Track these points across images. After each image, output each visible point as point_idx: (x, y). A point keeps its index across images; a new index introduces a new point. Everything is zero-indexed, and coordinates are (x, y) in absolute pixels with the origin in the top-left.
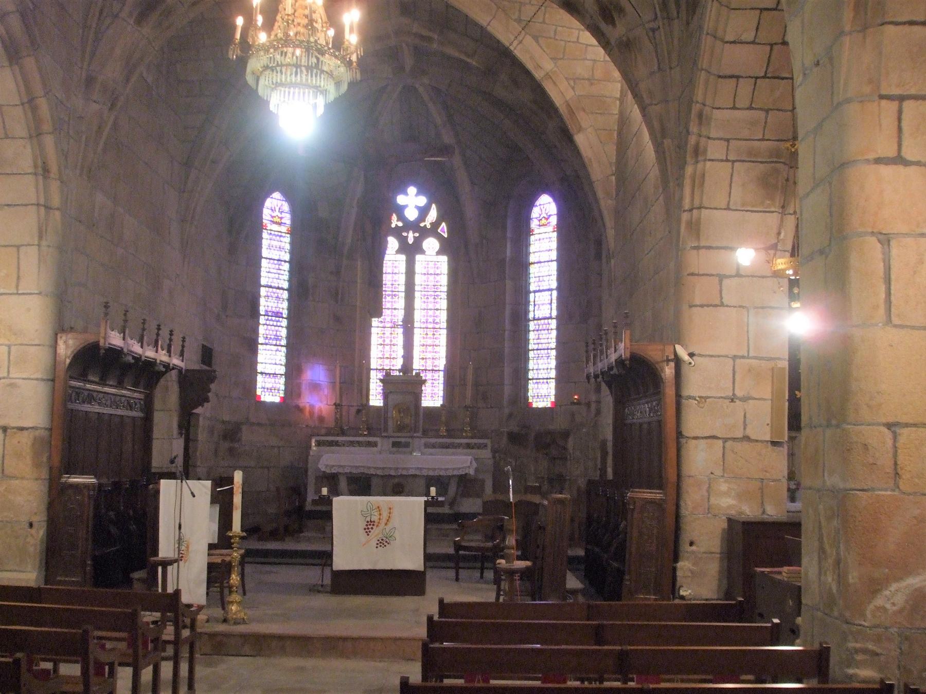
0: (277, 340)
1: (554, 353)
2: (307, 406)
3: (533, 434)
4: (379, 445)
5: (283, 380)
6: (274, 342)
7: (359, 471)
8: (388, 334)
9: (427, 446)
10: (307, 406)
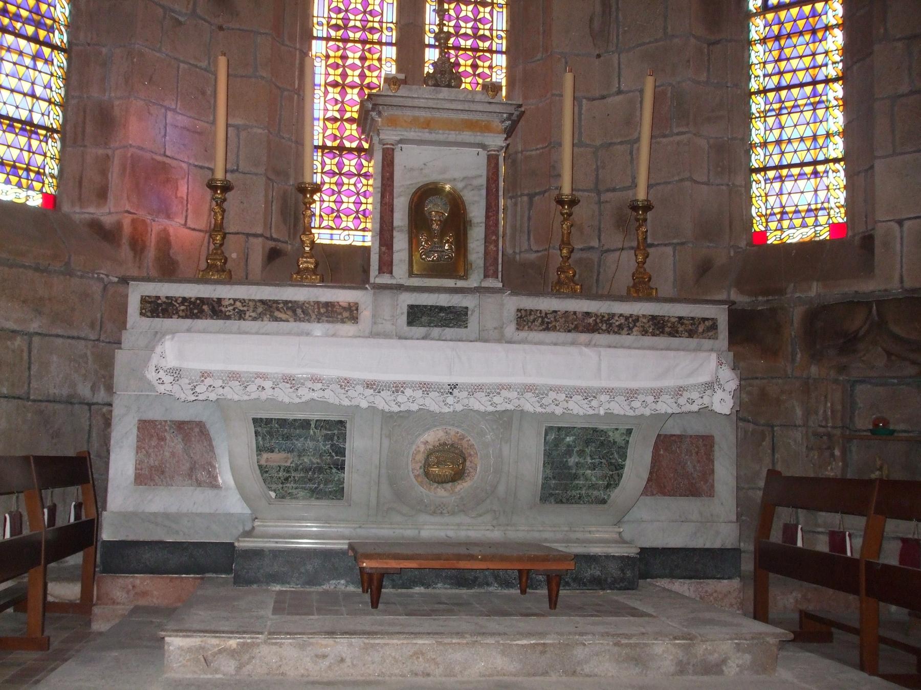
0: (39, 25)
1: (837, 90)
2: (127, 222)
3: (797, 314)
4: (365, 314)
5: (53, 147)
6: (30, 30)
7: (305, 395)
8: (354, 58)
9: (525, 320)
10: (127, 222)
